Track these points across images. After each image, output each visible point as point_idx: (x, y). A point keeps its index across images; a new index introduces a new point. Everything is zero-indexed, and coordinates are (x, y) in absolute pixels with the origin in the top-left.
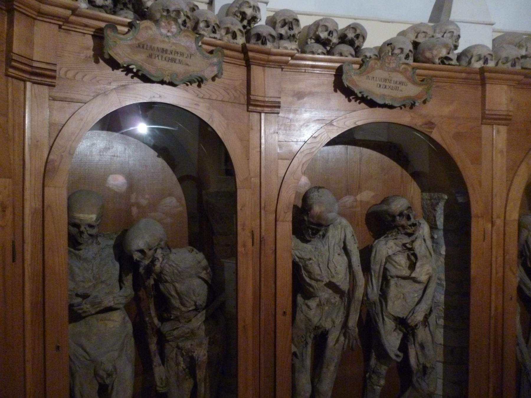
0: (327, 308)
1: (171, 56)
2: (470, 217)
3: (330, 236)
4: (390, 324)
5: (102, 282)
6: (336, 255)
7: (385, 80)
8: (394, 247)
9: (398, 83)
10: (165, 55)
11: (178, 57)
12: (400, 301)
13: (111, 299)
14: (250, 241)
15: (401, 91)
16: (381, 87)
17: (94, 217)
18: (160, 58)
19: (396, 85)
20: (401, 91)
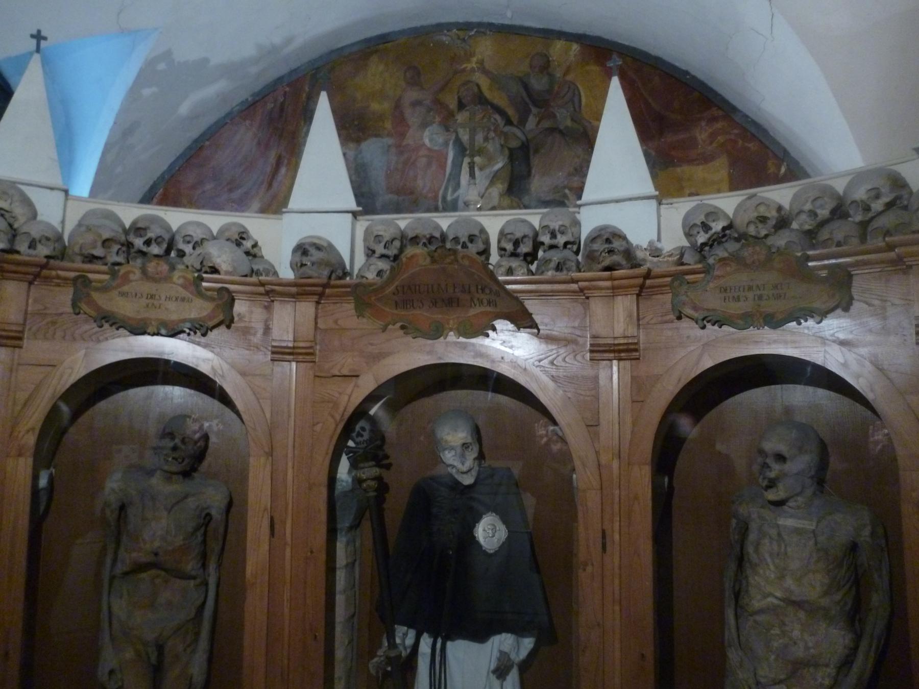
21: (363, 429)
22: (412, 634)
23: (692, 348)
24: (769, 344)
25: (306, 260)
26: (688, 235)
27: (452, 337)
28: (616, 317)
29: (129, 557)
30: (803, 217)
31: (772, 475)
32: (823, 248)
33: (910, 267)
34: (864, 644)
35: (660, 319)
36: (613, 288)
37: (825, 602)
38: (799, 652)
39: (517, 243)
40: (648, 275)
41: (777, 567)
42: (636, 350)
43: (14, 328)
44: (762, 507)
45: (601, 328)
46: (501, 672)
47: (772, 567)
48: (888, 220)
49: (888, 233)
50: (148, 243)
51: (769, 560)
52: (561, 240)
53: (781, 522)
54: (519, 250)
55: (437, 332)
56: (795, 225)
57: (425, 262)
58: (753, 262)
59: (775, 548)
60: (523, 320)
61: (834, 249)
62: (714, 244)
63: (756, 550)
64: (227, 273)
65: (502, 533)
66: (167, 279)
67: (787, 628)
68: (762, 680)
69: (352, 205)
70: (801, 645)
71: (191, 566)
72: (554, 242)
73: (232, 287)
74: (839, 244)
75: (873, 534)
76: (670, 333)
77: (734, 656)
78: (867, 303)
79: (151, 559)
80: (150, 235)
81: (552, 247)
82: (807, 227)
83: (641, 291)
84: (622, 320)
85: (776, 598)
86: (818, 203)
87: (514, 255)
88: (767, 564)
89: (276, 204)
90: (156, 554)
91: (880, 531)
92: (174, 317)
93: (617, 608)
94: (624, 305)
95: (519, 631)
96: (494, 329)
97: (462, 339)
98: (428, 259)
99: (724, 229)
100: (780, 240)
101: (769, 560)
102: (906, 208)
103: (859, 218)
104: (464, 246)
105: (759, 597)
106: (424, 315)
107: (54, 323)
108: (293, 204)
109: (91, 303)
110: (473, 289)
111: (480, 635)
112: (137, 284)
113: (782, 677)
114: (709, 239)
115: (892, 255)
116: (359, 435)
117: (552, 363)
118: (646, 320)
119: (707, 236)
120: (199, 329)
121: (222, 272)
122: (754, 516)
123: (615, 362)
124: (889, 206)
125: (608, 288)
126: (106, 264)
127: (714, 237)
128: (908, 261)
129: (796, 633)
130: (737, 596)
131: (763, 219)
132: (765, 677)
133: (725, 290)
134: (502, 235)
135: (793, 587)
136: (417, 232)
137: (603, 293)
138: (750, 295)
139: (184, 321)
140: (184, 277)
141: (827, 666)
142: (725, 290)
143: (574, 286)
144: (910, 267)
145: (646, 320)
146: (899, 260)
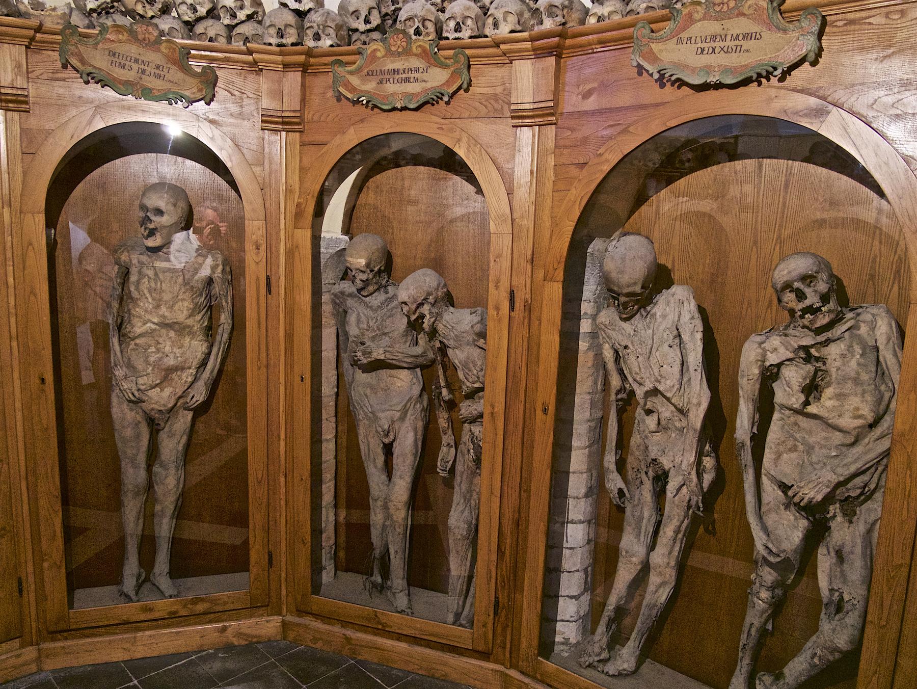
0: (673, 435)
1: (404, 76)
2: (564, 282)
3: (658, 314)
4: (771, 493)
5: (385, 334)
6: (666, 346)
7: (714, 38)
8: (782, 350)
9: (741, 37)
10: (397, 77)
11: (413, 75)
12: (793, 455)
13: (381, 352)
14: (506, 304)
15: (748, 51)
16: (705, 52)
17: (363, 262)
18: (392, 81)
19: (737, 42)
20: (748, 51)
23: (84, 108)
24: (155, 114)
31: (152, 226)
32: (199, 40)
33: (261, 70)
34: (215, 350)
35: (51, 75)
38: (170, 362)
40: (39, 29)
41: (154, 299)
42: (27, 103)
44: (141, 254)
47: (150, 300)
51: (148, 295)
58: (144, 39)
59: (153, 284)
61: (207, 43)
63: (137, 289)
67: (161, 346)
68: (142, 387)
70: (172, 356)
74: (211, 40)
75: (223, 270)
78: (230, 92)
83: (30, 44)
84: (9, 69)
85: (154, 323)
88: (146, 298)
91: (228, 269)
93: (14, 344)
101: (148, 295)
102: (260, 22)
103: (227, 21)
105: (140, 324)
113: (158, 381)
114: (99, 6)
115: (250, 58)
118: (38, 73)
122: (135, 261)
124: (249, 17)
127: (104, 6)
129: (168, 349)
130: (120, 327)
132: (145, 384)
133: (114, 55)
135: (166, 314)
138: (135, 67)
141: (190, 368)
142: (114, 55)
144: (261, 70)
145: (38, 73)
146: (255, 63)
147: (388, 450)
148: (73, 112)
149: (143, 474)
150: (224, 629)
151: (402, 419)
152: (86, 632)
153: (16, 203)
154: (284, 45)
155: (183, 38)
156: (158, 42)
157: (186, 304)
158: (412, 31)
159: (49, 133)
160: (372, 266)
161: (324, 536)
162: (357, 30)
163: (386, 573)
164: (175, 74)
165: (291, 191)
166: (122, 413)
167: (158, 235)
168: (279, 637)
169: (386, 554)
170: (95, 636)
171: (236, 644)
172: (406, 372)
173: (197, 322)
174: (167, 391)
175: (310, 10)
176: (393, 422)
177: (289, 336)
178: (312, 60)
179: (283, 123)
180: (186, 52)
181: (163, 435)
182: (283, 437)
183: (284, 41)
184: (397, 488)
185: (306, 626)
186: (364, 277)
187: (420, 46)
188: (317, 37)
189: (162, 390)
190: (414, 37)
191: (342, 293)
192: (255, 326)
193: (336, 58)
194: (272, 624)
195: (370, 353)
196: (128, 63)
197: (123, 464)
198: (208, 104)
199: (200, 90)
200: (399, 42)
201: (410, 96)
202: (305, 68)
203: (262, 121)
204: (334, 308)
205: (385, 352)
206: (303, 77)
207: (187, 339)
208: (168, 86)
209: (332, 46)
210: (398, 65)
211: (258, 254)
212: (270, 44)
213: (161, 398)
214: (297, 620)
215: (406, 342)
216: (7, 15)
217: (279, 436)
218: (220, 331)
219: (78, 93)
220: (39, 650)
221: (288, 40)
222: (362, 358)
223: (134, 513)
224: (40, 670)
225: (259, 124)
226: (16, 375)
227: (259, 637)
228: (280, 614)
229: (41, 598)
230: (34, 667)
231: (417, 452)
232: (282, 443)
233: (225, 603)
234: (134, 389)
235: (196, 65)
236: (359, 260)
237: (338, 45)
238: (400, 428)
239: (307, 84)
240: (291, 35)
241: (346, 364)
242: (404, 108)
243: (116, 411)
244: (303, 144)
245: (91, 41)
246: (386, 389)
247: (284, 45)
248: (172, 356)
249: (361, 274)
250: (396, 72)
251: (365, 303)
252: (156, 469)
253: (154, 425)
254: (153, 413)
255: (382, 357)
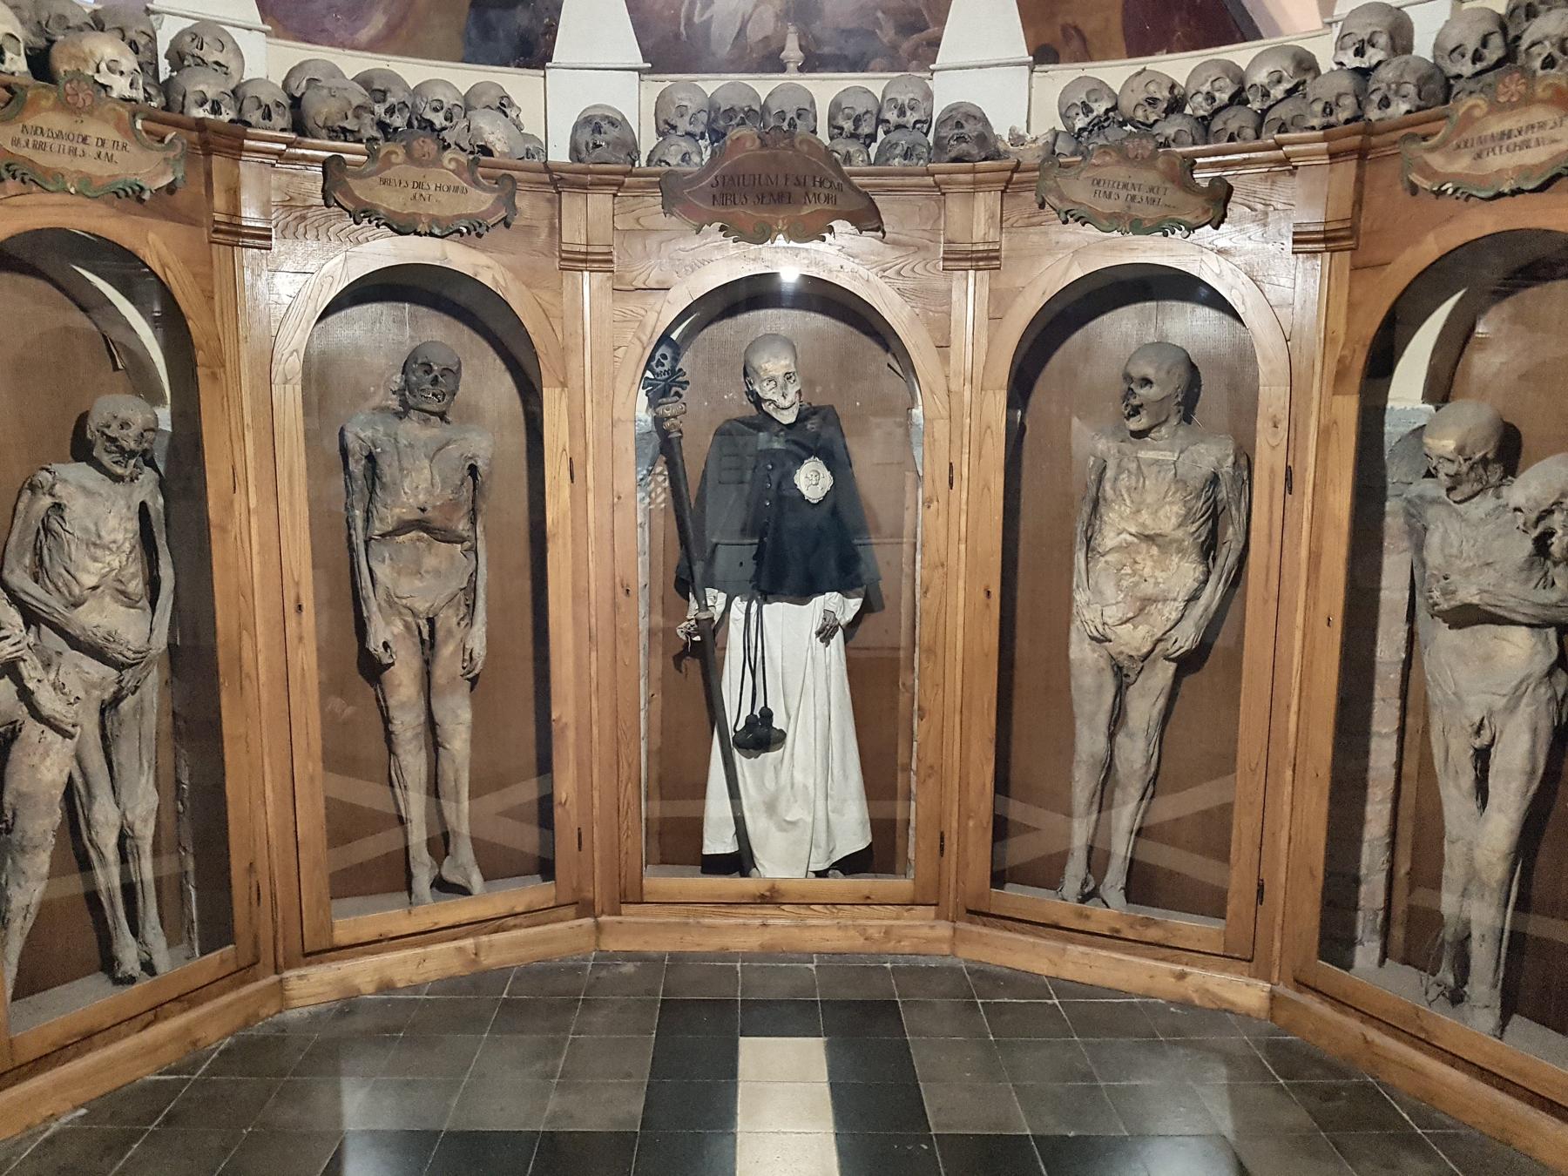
10: (1507, 142)
21: (664, 357)
22: (722, 598)
25: (599, 139)
26: (1064, 116)
27: (781, 241)
28: (977, 218)
29: (389, 515)
30: (1200, 98)
31: (1136, 402)
34: (1213, 578)
36: (974, 183)
37: (1180, 534)
38: (1148, 589)
39: (857, 121)
42: (997, 258)
43: (1311, 229)
45: (955, 231)
46: (825, 634)
48: (1283, 112)
49: (1282, 129)
50: (391, 111)
52: (911, 118)
53: (1142, 454)
54: (860, 131)
55: (761, 235)
56: (1188, 110)
57: (752, 145)
60: (867, 218)
62: (1097, 128)
64: (503, 154)
65: (827, 481)
66: (437, 163)
68: (1110, 621)
69: (637, 59)
70: (1152, 581)
71: (462, 526)
72: (902, 120)
73: (515, 174)
76: (1035, 238)
77: (1080, 597)
79: (418, 515)
80: (391, 100)
81: (898, 127)
82: (1202, 113)
86: (1217, 84)
87: (854, 136)
89: (533, 52)
90: (423, 510)
92: (448, 213)
93: (963, 547)
94: (986, 203)
95: (845, 589)
96: (831, 230)
97: (792, 244)
98: (758, 142)
99: (1107, 111)
100: (1169, 128)
103: (1256, 105)
104: (792, 125)
105: (1112, 534)
106: (746, 213)
107: (303, 218)
108: (558, 56)
109: (348, 194)
110: (809, 182)
111: (802, 595)
112: (400, 167)
113: (1131, 615)
116: (660, 364)
117: (899, 273)
119: (1087, 120)
120: (471, 230)
121: (496, 154)
123: (971, 273)
124: (1290, 93)
125: (967, 183)
126: (360, 141)
128: (1295, 161)
131: (1152, 102)
134: (836, 108)
136: (733, 103)
137: (964, 188)
138: (1123, 193)
139: (459, 217)
140: (457, 161)
143: (930, 180)
144: (1296, 167)
146: (1286, 160)
147: (1482, 757)
148: (1048, 261)
149: (1101, 742)
150: (1182, 976)
151: (1511, 709)
152: (1009, 923)
153: (977, 381)
154: (1332, 126)
155: (1194, 143)
156: (1153, 156)
157: (1175, 508)
158: (1537, 63)
159: (1020, 291)
160: (1468, 451)
161: (1363, 888)
162: (1459, 76)
163: (1463, 968)
164: (1174, 195)
165: (1333, 339)
166: (1081, 651)
167: (1143, 412)
168: (1263, 1015)
169: (1464, 941)
170: (1016, 931)
171: (1197, 1002)
172: (1523, 631)
173: (1193, 532)
174: (1142, 630)
175: (1380, 63)
176: (1491, 713)
177: (1315, 558)
178: (1374, 140)
179: (1325, 240)
180: (1190, 164)
181: (1133, 694)
182: (1294, 708)
183: (1332, 119)
184: (1490, 827)
185: (1306, 1008)
186: (1452, 469)
187: (1550, 85)
188: (1385, 103)
189: (1135, 627)
190: (1540, 73)
191: (1421, 497)
192: (1264, 540)
193: (1413, 130)
194: (1251, 991)
195: (1454, 592)
196: (1115, 191)
197: (1078, 723)
198: (1217, 228)
199: (1206, 212)
200: (1513, 87)
201: (1525, 171)
202: (1362, 154)
203: (1294, 242)
204: (1407, 523)
205: (1482, 591)
206: (1360, 166)
207: (1175, 559)
208: (1165, 211)
209: (1409, 112)
210: (1509, 123)
211: (1275, 435)
212: (1313, 128)
213: (1133, 639)
214: (1291, 994)
215: (1528, 580)
216: (985, 159)
217: (1288, 707)
218: (1224, 551)
219: (1054, 237)
220: (955, 930)
221: (1343, 115)
222: (1441, 600)
223: (1087, 794)
224: (954, 954)
225: (1289, 245)
226: (961, 584)
227: (1233, 1004)
228: (1269, 981)
229: (962, 866)
230: (946, 949)
231: (1533, 772)
232: (1293, 718)
233: (1188, 939)
234: (1098, 622)
235: (1202, 177)
236: (1445, 442)
237: (1419, 109)
238: (1504, 725)
239: (1367, 177)
240: (1345, 108)
241: (1422, 614)
242: (1519, 191)
243: (1074, 653)
244: (1354, 268)
245: (1072, 172)
246: (1487, 658)
247: (1332, 126)
248: (1152, 581)
249: (1448, 464)
250: (1507, 135)
251: (1459, 514)
252: (1120, 738)
253: (1122, 675)
254: (1121, 658)
255: (1475, 600)
